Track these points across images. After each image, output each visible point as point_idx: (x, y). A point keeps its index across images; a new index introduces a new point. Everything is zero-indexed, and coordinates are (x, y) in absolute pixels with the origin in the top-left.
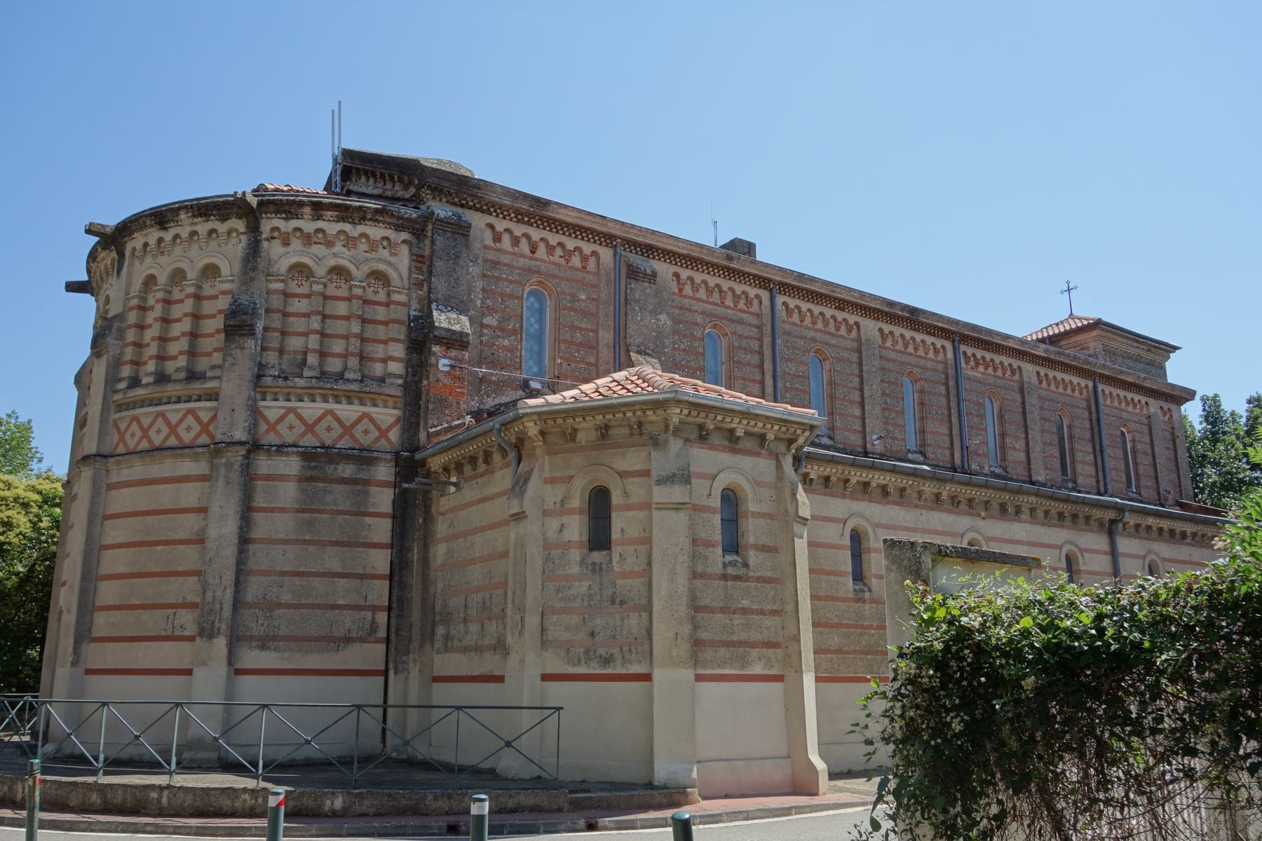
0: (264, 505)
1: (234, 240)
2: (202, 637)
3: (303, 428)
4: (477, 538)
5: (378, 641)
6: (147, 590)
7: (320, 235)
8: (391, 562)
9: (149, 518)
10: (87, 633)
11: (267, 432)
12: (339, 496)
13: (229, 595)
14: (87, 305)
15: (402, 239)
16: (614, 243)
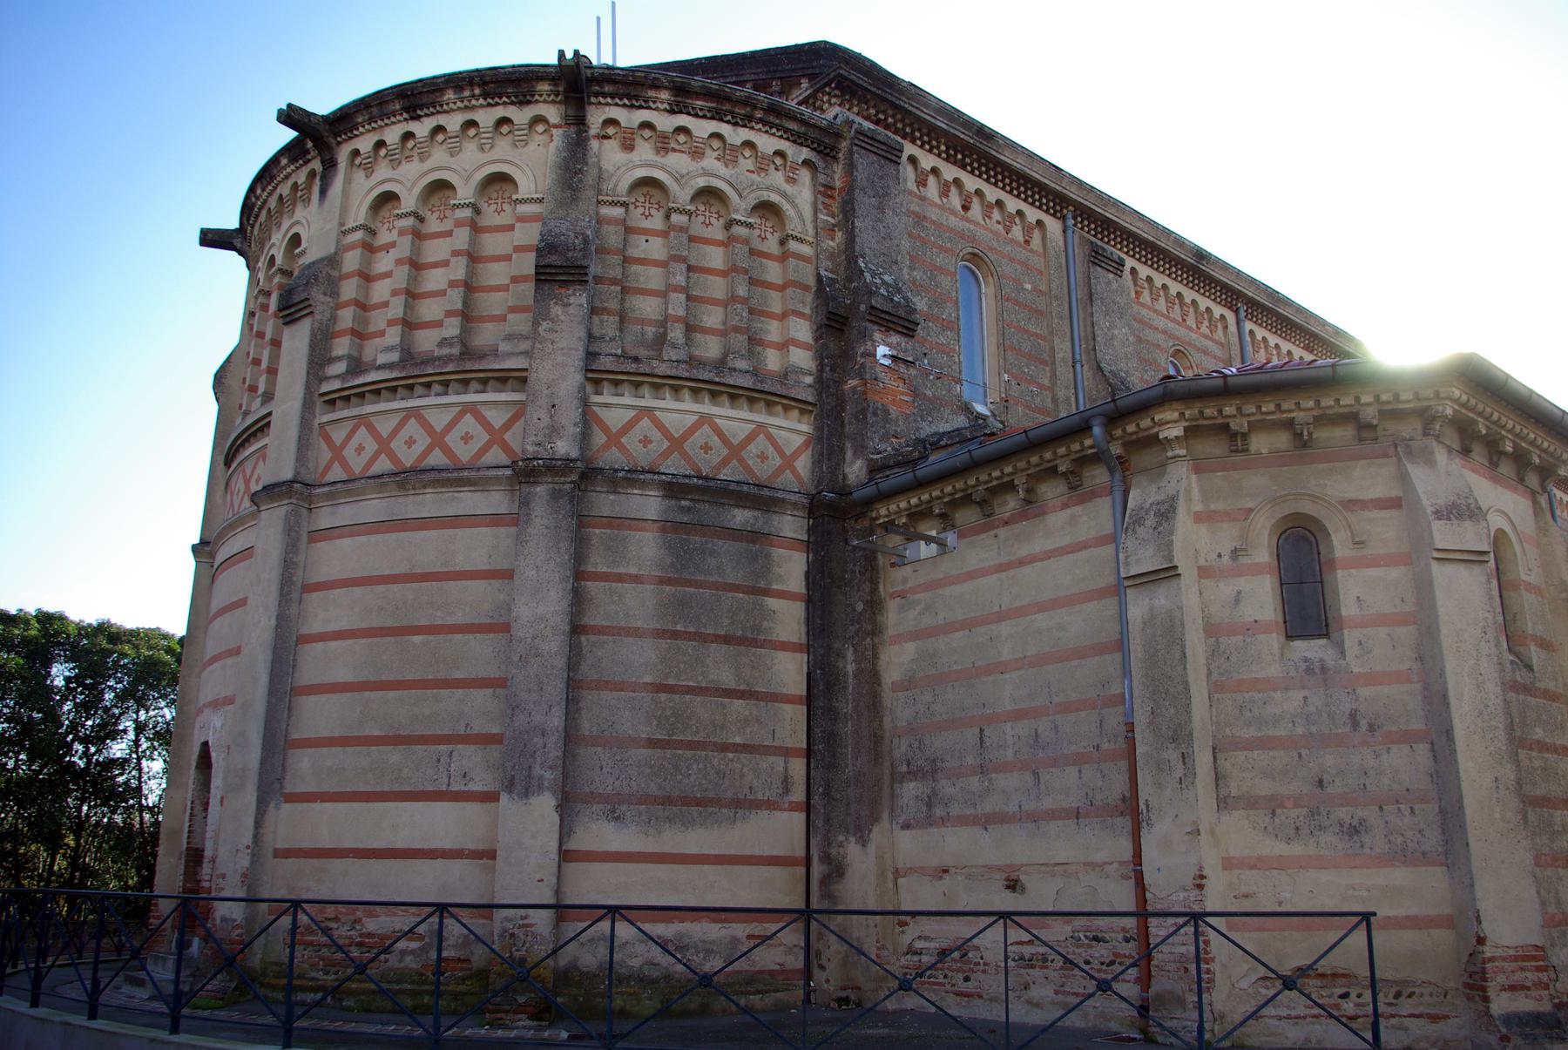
0: (605, 569)
1: (538, 138)
2: (511, 792)
3: (666, 444)
4: (1005, 629)
5: (794, 807)
6: (398, 710)
7: (682, 138)
8: (809, 674)
9: (394, 587)
10: (277, 785)
11: (606, 447)
12: (725, 561)
13: (556, 720)
14: (231, 269)
15: (803, 158)
16: (1065, 211)
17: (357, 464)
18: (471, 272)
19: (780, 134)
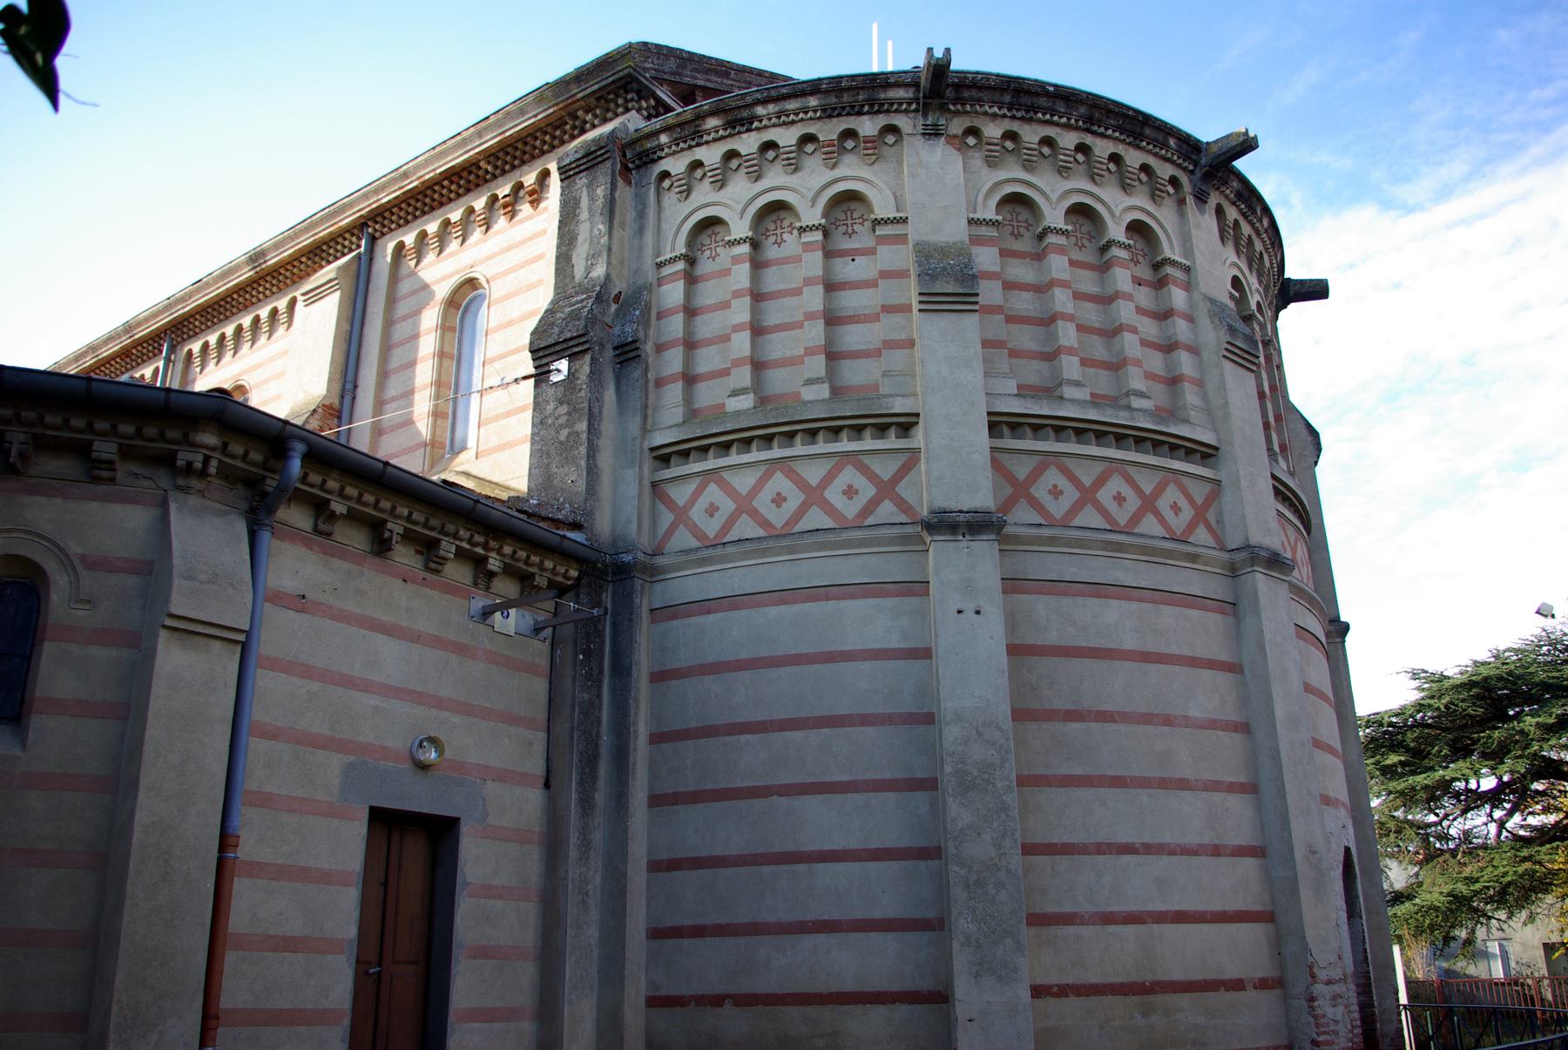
17: (778, 517)
18: (755, 312)
19: (1122, 137)
